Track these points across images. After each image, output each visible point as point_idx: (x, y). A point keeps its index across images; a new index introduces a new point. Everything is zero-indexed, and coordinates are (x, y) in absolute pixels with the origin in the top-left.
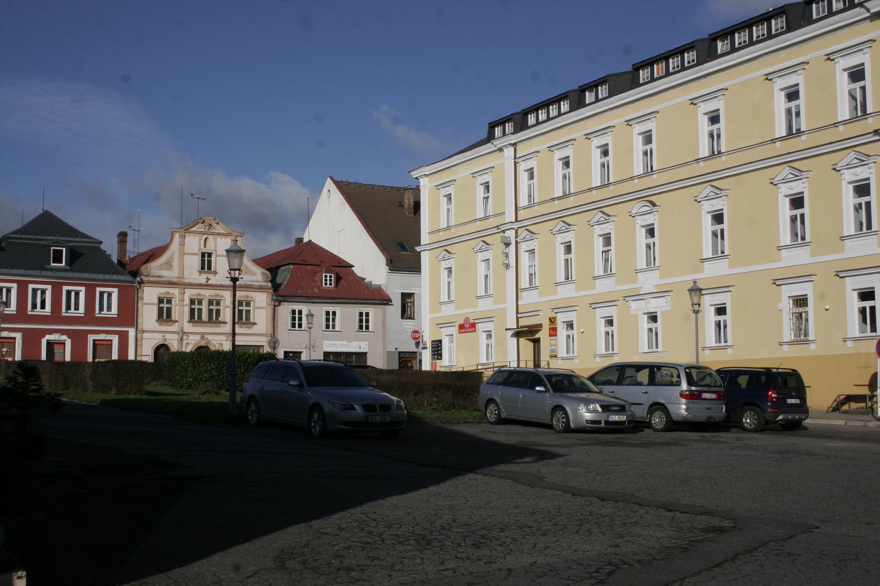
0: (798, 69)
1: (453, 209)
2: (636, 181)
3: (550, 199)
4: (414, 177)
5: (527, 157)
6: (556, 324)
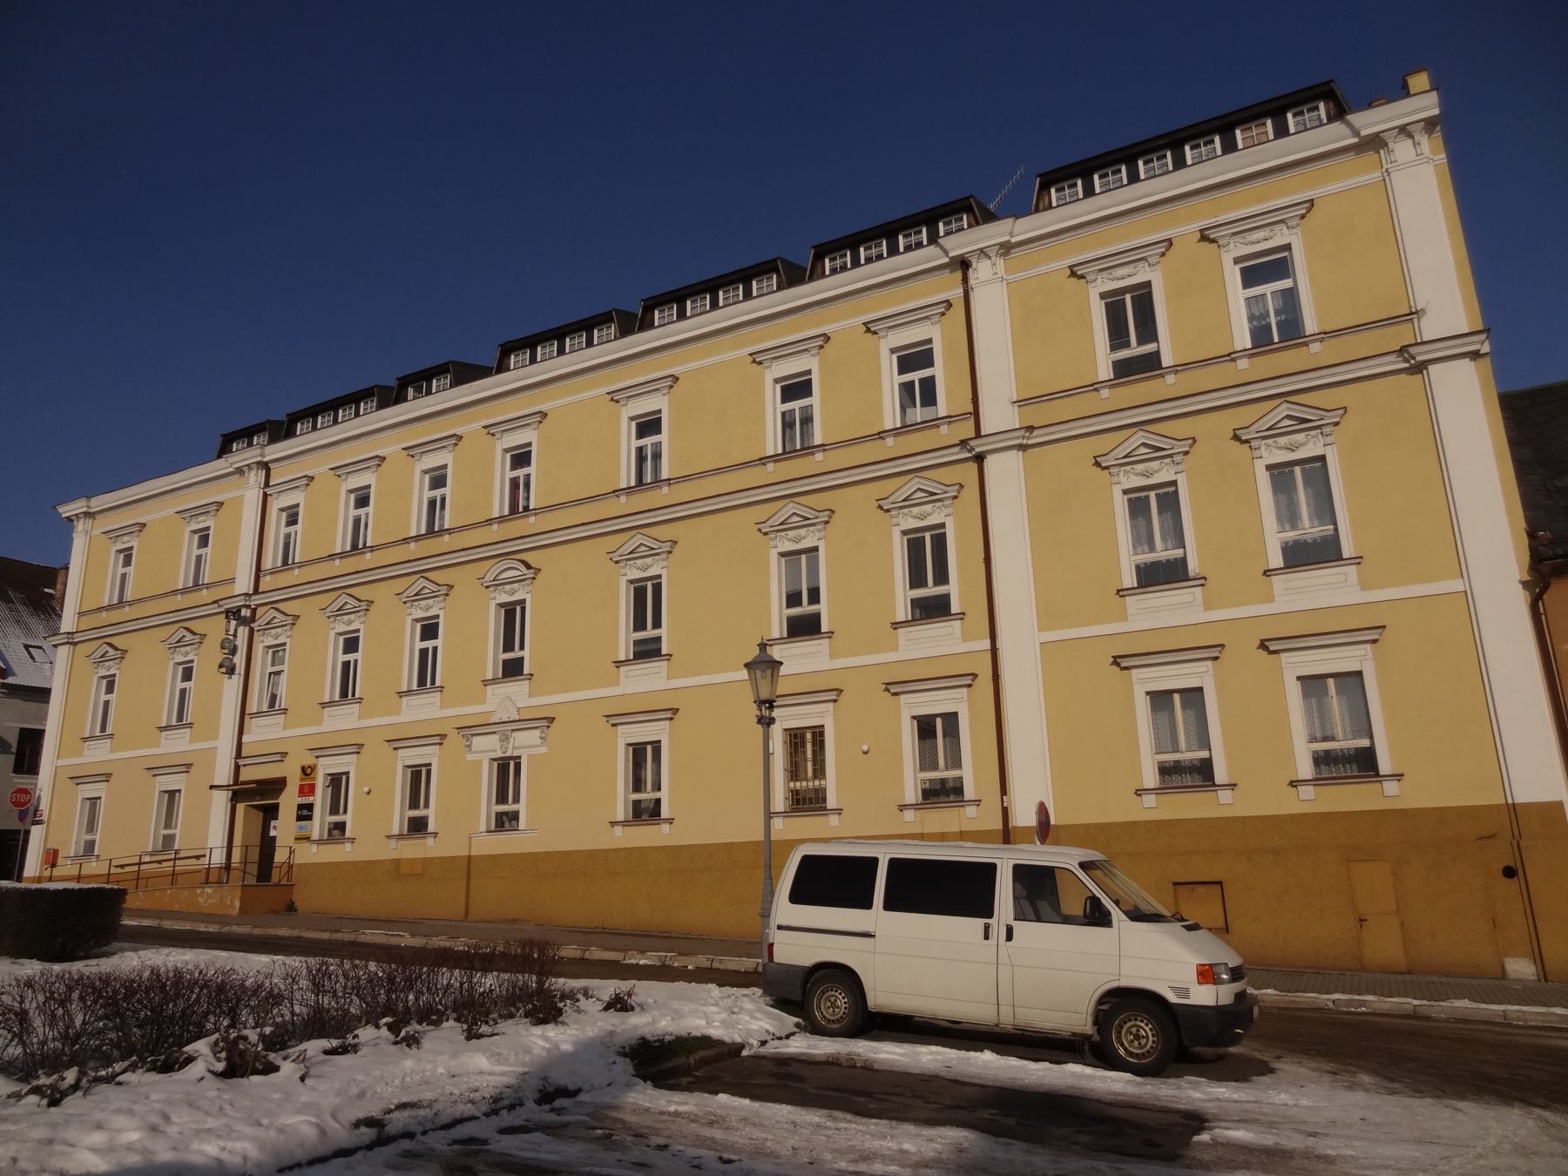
0: (1149, 253)
1: (132, 573)
2: (495, 527)
3: (327, 555)
4: (64, 515)
5: (290, 485)
6: (313, 779)
